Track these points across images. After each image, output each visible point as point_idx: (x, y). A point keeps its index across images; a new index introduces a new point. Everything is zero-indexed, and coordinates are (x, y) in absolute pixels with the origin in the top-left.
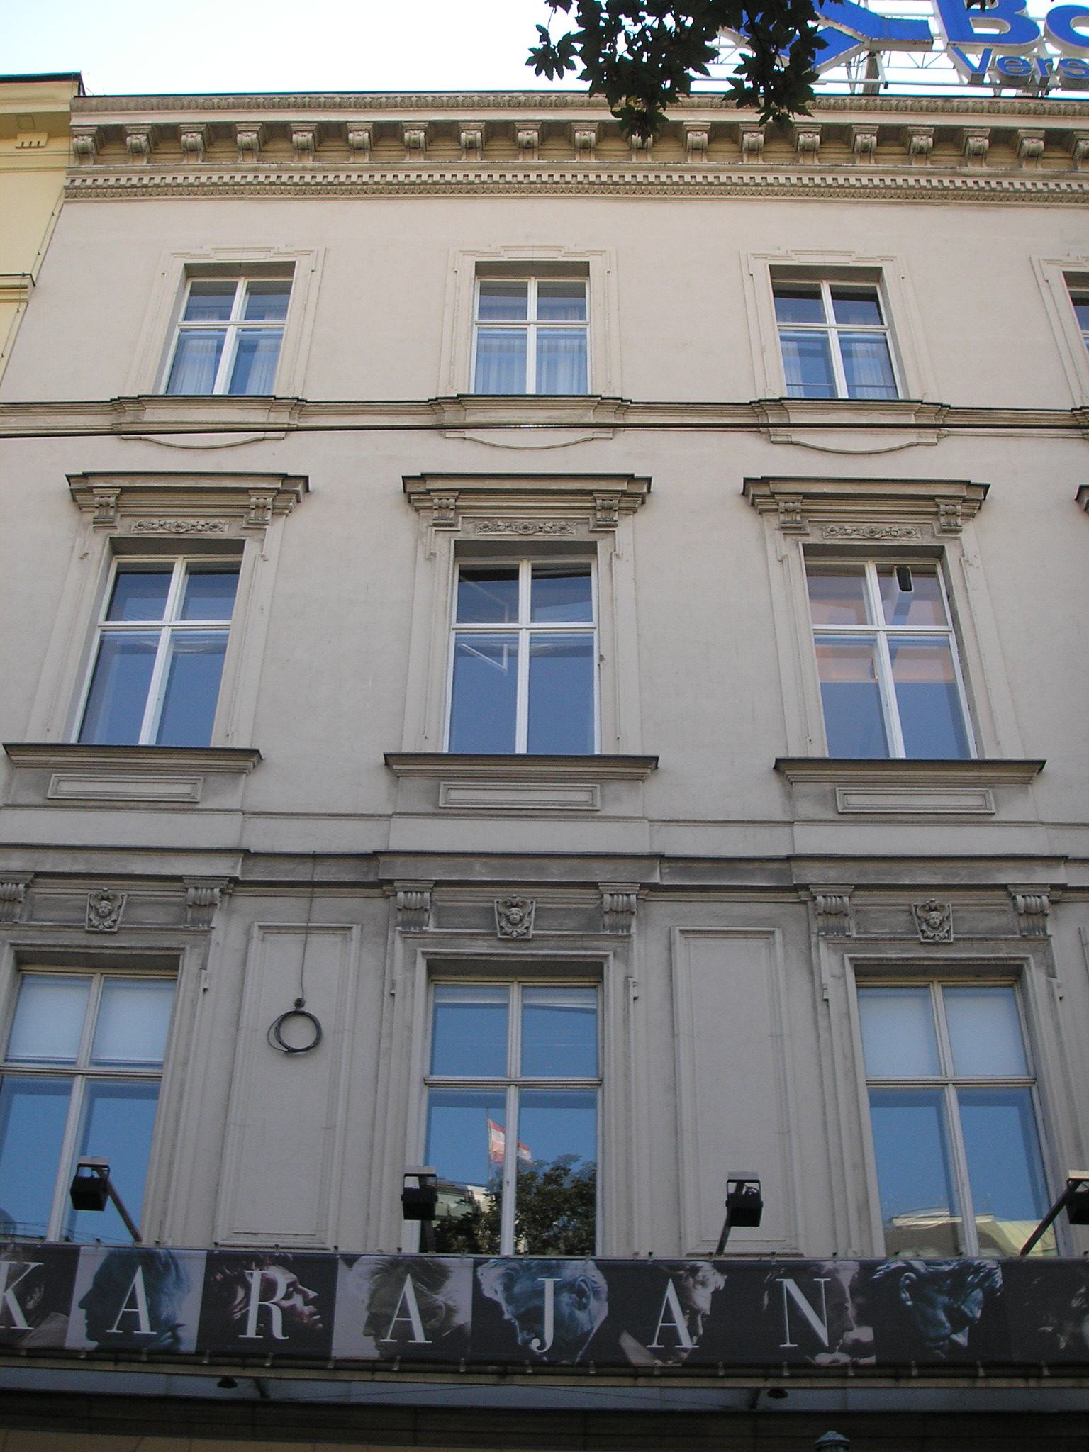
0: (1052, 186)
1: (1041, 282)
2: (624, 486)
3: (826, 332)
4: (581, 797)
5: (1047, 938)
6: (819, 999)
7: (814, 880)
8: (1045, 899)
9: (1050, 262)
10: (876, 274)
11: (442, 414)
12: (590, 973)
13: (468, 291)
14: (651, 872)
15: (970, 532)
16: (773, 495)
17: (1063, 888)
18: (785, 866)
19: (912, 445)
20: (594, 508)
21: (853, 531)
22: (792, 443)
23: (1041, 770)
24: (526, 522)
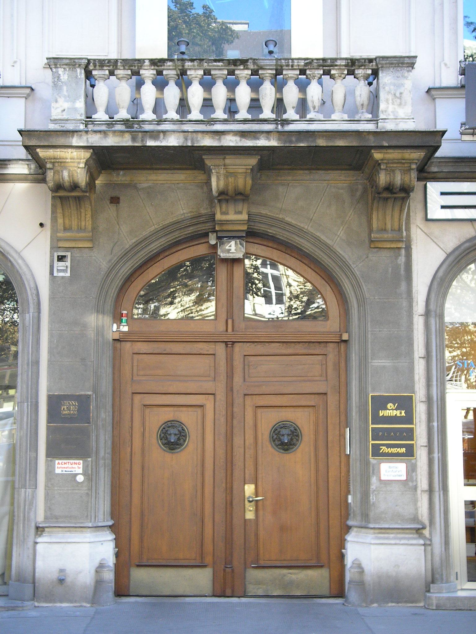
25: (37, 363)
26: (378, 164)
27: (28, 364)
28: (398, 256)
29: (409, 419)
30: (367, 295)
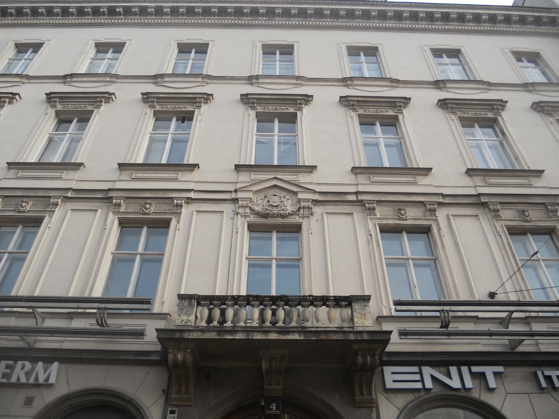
9: (343, 43)
11: (251, 79)
12: (165, 224)
16: (148, 98)
23: (199, 167)
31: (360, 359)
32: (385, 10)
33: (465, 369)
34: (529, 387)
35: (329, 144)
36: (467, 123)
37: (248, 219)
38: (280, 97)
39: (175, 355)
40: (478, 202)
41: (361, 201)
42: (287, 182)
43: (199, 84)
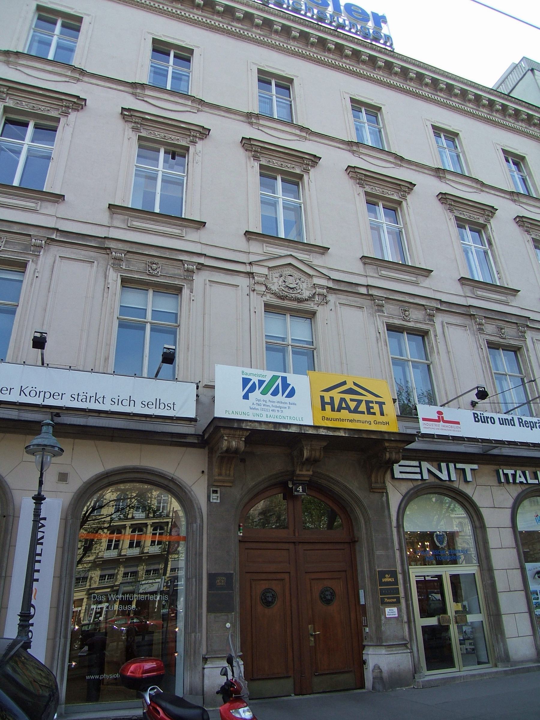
0: (262, 38)
1: (249, 69)
2: (75, 100)
3: (168, 68)
4: (503, 298)
5: (193, 280)
6: (106, 287)
7: (113, 247)
8: (195, 267)
10: (191, 51)
13: (31, 15)
14: (53, 234)
15: (200, 145)
16: (131, 116)
17: (202, 265)
18: (103, 240)
19: (187, 111)
20: (62, 106)
21: (158, 135)
22: (144, 100)
23: (204, 226)
24: (34, 105)
25: (201, 554)
26: (385, 449)
27: (196, 554)
28: (383, 496)
29: (396, 583)
30: (371, 517)
31: (388, 455)
32: (393, 63)
33: (451, 465)
34: (493, 481)
35: (222, 191)
36: (461, 223)
37: (265, 299)
38: (287, 151)
39: (229, 442)
40: (467, 313)
41: (372, 295)
42: (301, 261)
43: (189, 109)
